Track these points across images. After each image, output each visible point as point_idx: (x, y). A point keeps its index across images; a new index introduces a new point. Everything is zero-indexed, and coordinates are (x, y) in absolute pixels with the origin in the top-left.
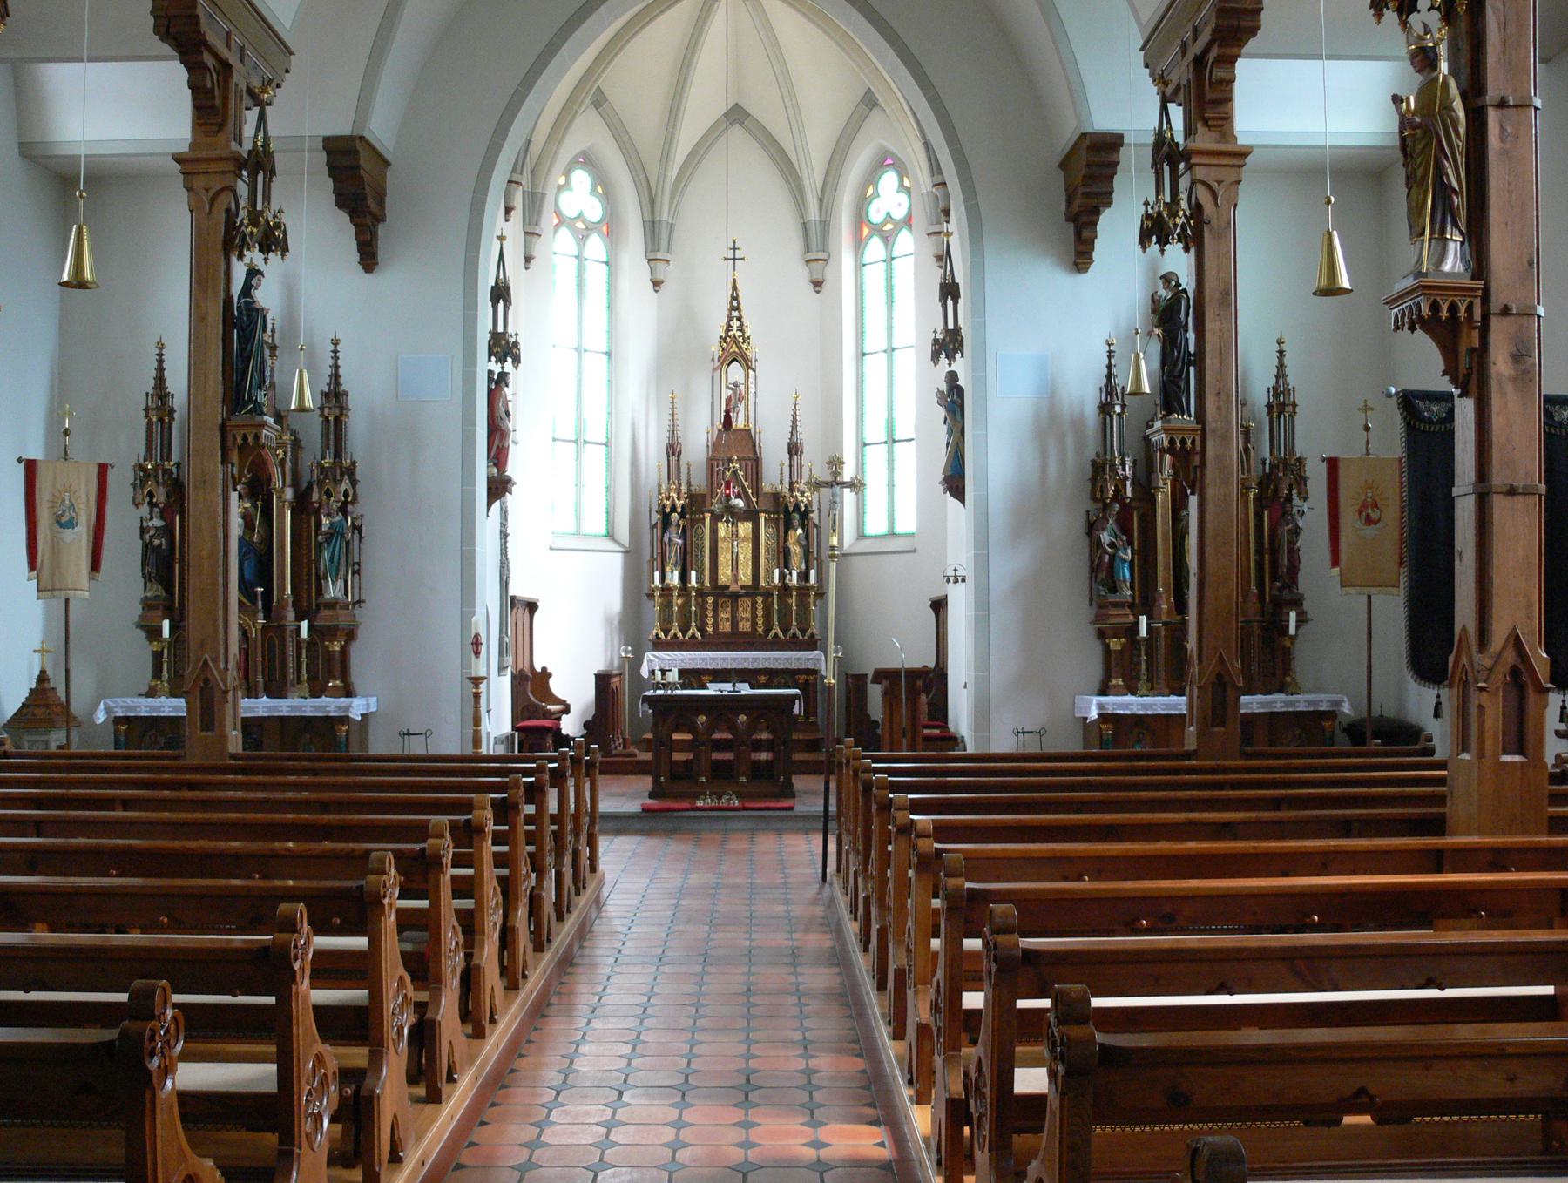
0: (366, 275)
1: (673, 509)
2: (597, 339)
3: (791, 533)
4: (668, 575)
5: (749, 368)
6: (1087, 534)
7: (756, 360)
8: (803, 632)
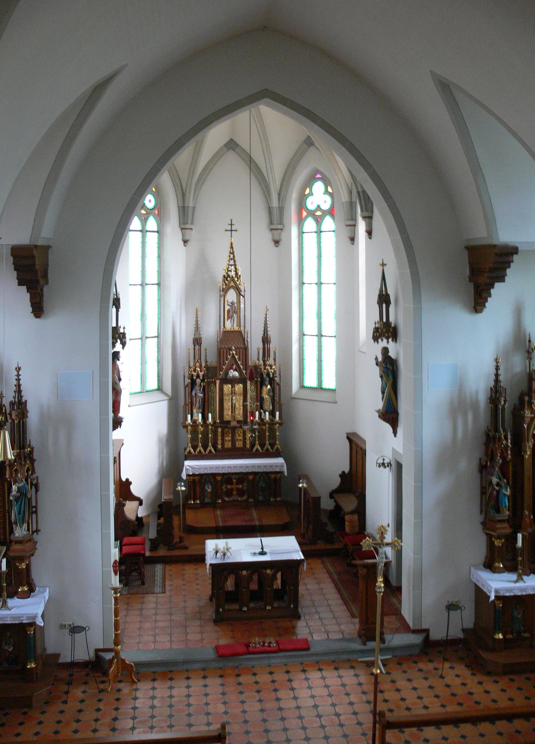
0: (37, 319)
1: (198, 376)
2: (152, 277)
3: (264, 388)
5: (240, 295)
6: (479, 471)
7: (245, 291)
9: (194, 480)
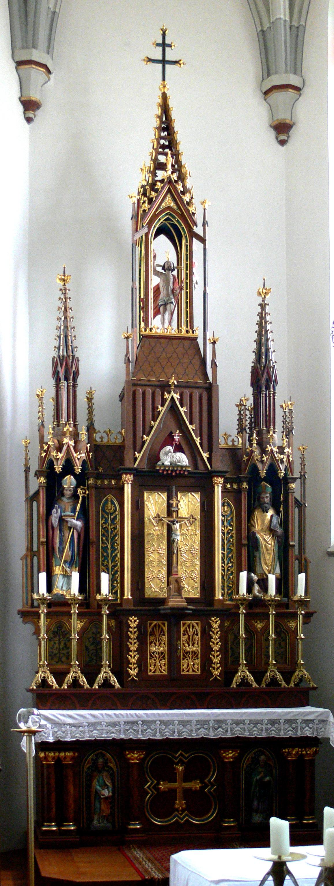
1: (68, 467)
4: (59, 582)
7: (205, 224)
8: (287, 676)
9: (58, 760)
